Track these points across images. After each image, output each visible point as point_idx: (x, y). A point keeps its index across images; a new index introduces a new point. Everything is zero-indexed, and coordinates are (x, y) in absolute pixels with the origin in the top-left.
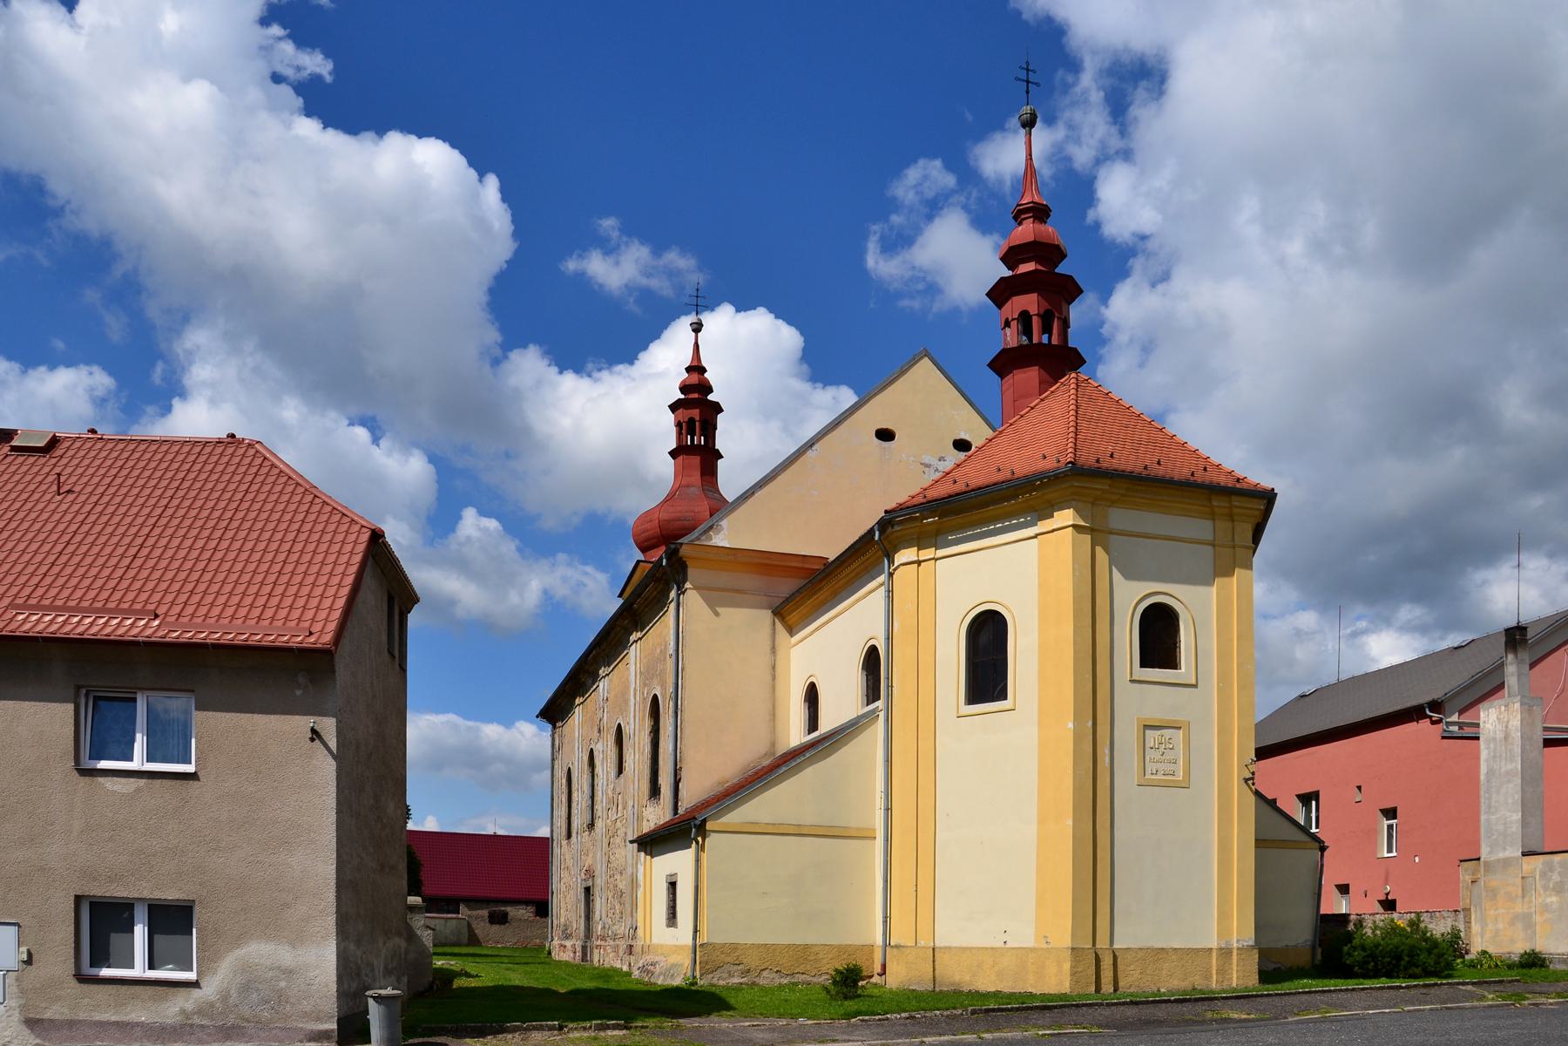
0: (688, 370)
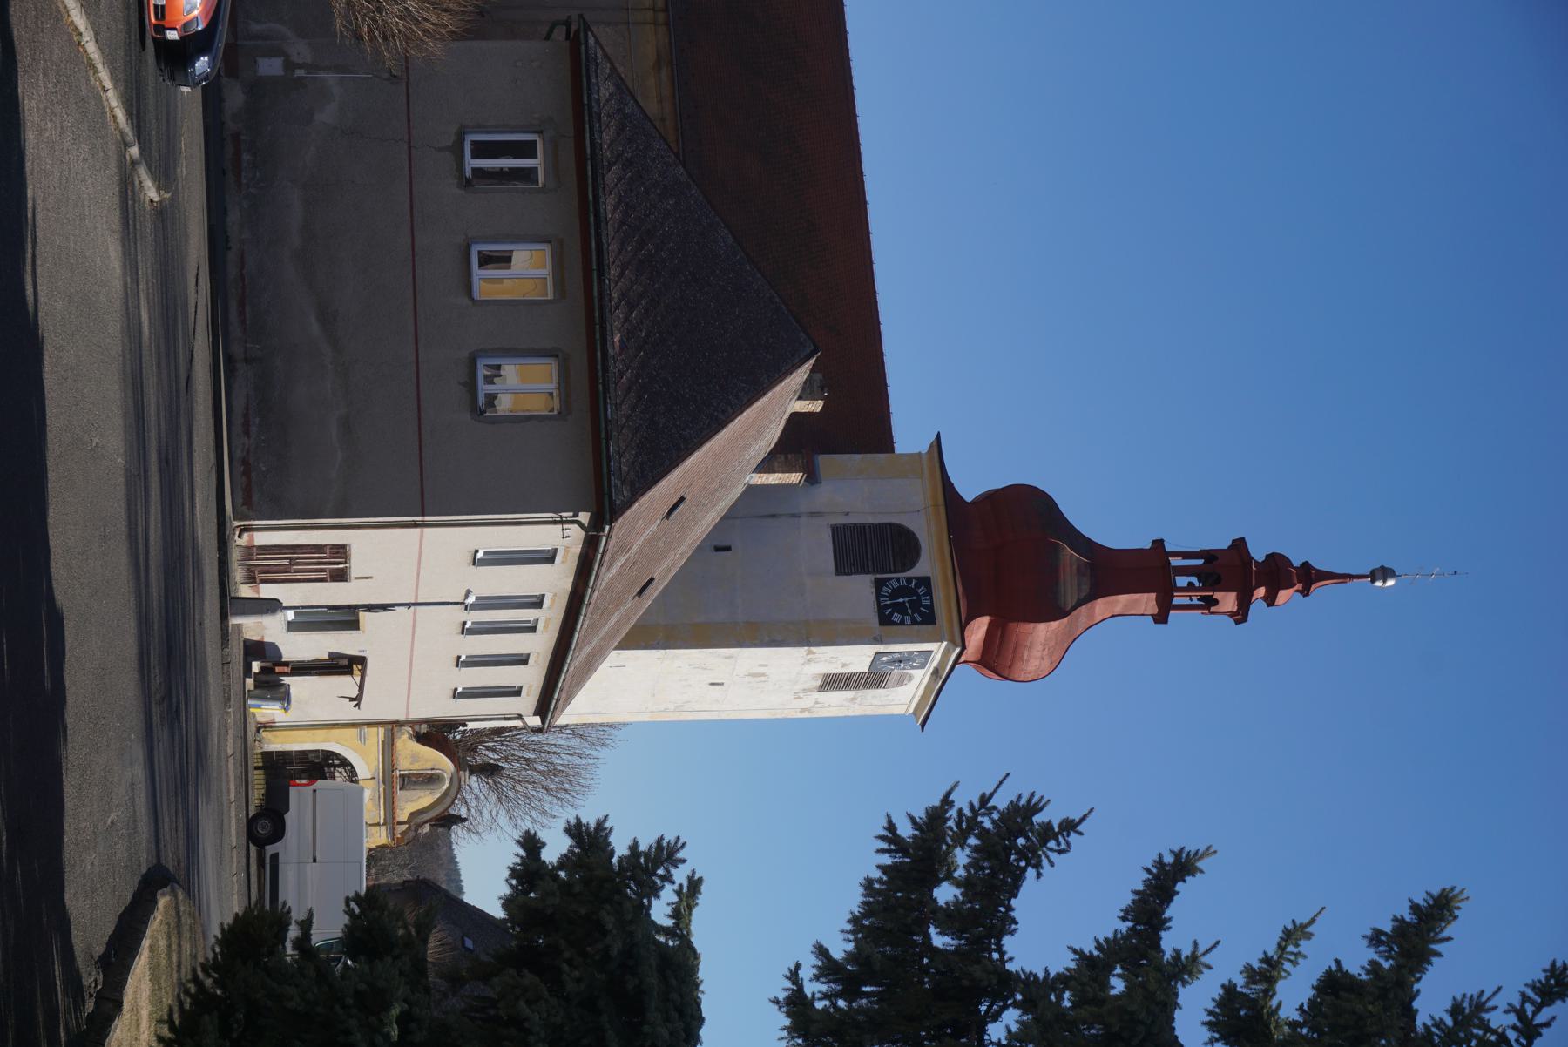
0: (1306, 565)
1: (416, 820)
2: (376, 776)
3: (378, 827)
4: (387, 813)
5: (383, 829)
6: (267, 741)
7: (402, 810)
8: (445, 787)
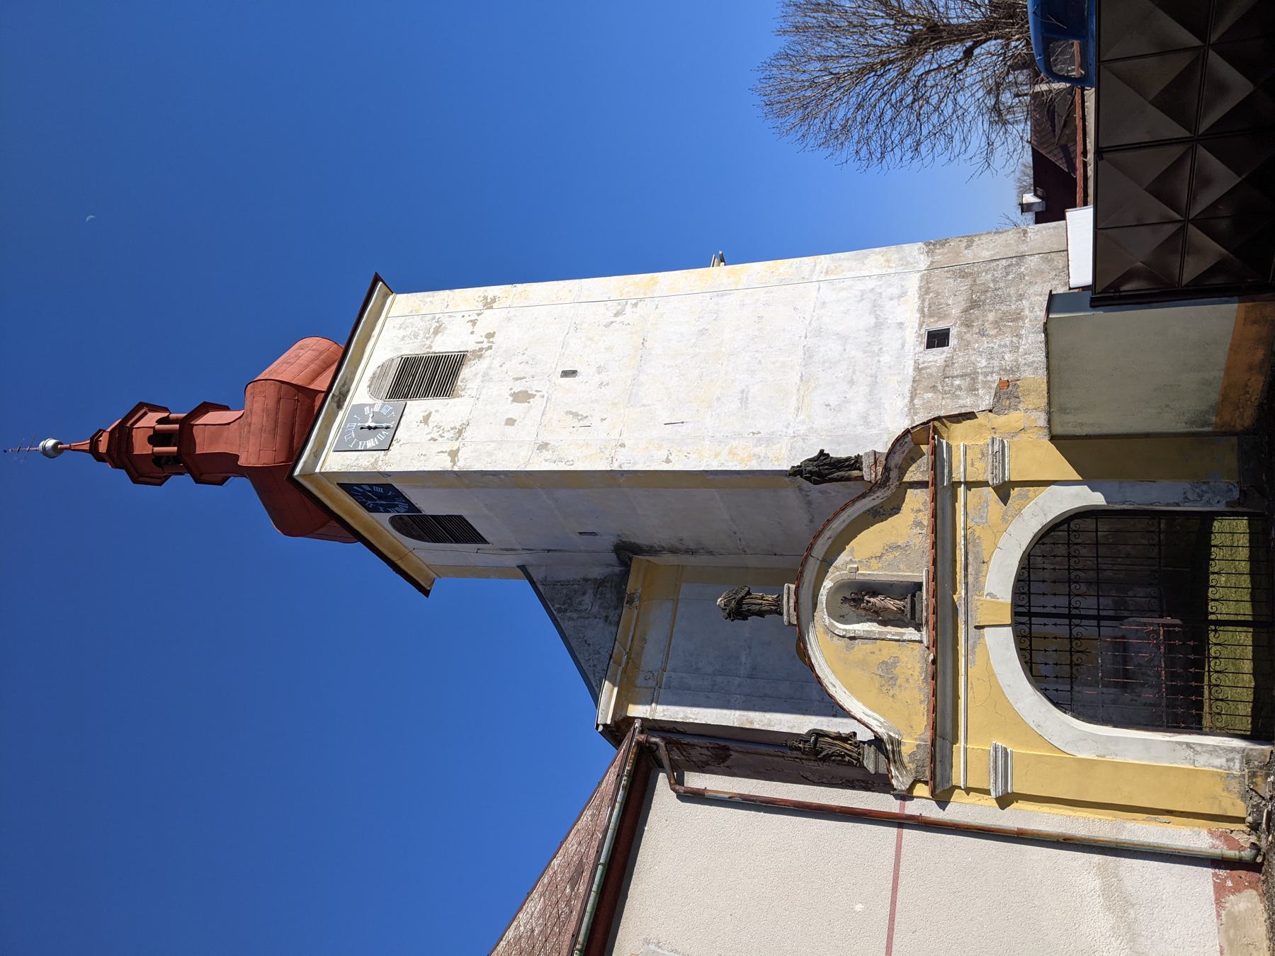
1: (889, 493)
2: (972, 631)
3: (969, 479)
4: (949, 555)
5: (958, 475)
6: (1235, 785)
7: (918, 524)
8: (828, 584)
